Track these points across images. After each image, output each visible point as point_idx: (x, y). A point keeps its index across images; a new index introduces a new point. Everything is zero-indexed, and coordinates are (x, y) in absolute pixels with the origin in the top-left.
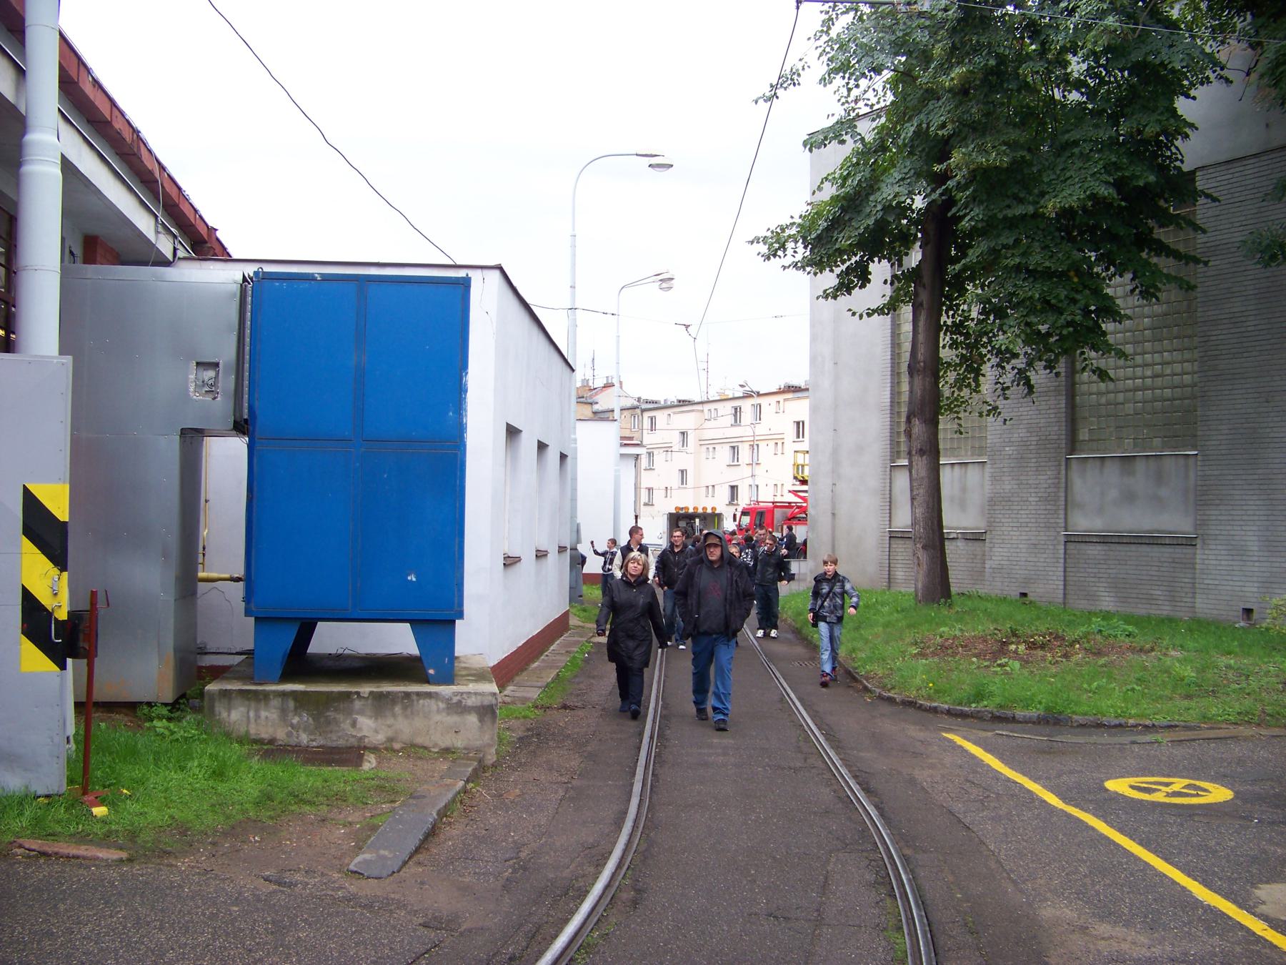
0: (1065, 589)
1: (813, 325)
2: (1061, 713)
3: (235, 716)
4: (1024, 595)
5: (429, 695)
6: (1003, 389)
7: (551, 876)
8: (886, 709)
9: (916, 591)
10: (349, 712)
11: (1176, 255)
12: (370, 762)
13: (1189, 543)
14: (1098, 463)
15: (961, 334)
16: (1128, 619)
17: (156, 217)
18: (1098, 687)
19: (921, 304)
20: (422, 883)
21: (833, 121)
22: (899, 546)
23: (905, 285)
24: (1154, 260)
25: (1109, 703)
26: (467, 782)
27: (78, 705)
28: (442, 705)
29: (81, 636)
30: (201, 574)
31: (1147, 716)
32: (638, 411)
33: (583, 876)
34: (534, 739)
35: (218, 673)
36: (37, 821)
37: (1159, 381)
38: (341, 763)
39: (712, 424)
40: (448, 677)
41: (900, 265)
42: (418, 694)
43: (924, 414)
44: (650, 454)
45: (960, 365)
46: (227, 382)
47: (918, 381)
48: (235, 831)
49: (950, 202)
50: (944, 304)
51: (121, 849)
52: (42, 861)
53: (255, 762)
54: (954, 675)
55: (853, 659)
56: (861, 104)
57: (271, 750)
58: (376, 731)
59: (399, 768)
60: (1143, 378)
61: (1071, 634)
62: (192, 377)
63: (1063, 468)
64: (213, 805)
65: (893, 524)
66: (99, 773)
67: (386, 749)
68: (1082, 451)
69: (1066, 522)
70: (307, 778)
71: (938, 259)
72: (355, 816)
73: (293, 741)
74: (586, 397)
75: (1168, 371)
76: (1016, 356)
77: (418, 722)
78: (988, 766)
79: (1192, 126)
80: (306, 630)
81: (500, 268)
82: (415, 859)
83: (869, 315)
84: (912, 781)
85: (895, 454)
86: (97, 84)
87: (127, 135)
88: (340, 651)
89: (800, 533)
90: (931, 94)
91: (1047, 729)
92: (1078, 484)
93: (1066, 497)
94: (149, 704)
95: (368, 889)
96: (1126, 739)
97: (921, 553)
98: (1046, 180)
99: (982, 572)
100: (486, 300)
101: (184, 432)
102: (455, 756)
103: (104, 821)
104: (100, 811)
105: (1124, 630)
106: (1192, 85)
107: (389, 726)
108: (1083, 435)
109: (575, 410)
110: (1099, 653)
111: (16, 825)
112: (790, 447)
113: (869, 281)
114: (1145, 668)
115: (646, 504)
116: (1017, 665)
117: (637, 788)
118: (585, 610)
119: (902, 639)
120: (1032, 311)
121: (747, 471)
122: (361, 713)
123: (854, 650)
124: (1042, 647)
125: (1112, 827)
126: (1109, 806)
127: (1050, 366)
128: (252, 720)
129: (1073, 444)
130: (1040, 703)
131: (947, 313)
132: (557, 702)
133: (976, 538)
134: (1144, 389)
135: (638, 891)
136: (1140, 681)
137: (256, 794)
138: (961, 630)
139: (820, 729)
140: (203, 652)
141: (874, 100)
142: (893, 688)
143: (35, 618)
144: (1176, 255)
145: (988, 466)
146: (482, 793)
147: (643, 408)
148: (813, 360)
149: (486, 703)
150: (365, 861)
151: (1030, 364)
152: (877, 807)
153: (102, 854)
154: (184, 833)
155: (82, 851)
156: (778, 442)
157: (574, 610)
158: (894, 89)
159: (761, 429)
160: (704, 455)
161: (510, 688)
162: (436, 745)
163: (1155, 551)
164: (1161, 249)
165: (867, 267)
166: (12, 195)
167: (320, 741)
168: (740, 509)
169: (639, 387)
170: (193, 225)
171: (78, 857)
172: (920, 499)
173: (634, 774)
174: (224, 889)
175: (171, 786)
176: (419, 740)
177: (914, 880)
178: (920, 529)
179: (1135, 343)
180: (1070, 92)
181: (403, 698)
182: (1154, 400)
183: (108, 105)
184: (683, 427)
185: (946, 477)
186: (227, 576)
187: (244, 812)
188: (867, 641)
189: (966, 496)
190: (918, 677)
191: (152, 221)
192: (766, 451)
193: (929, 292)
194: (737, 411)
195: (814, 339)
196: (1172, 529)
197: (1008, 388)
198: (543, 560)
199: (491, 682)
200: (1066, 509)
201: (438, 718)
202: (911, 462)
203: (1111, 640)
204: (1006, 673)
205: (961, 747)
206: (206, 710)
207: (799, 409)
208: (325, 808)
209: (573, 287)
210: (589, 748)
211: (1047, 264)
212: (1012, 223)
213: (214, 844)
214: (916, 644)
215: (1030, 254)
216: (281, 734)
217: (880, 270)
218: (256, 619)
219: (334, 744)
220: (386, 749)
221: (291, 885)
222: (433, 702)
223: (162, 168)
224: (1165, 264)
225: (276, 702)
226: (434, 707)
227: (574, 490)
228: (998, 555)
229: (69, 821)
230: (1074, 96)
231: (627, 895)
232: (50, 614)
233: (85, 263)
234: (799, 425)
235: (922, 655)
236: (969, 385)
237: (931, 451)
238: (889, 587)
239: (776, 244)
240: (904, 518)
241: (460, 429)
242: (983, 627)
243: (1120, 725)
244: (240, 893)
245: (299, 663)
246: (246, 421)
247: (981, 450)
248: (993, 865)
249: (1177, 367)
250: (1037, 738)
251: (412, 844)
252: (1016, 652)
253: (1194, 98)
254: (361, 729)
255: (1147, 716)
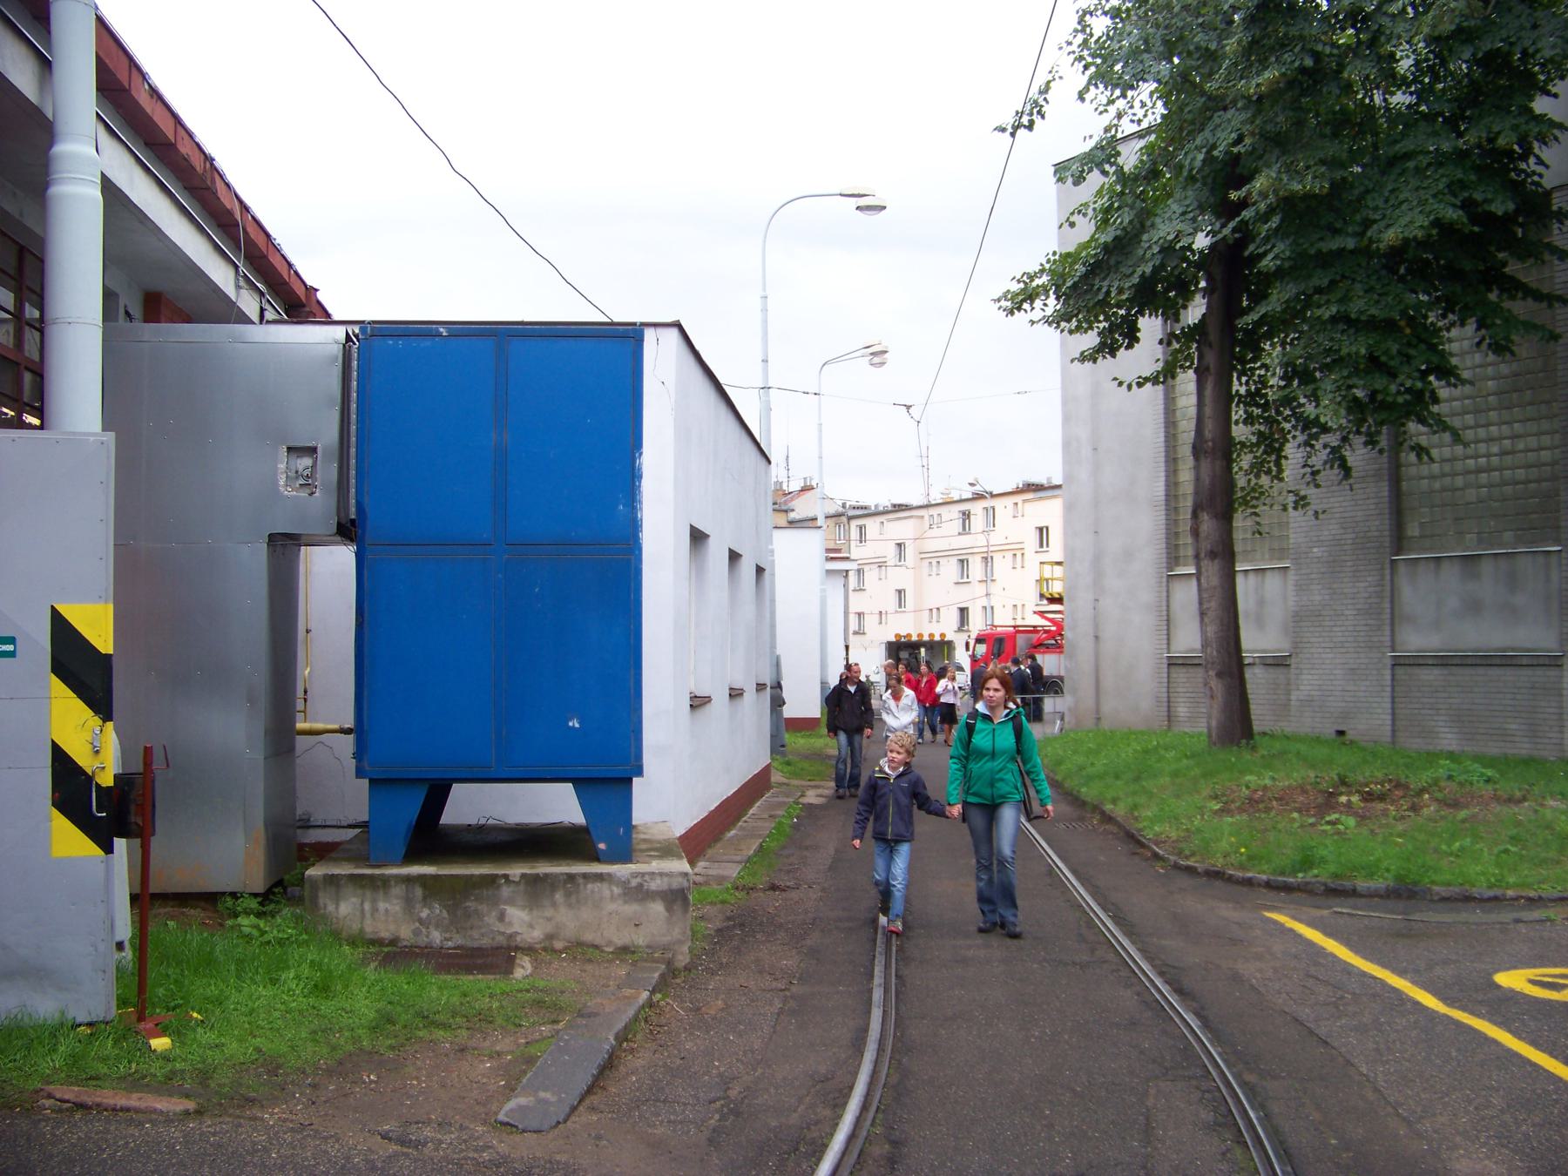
0: (1393, 724)
1: (1065, 403)
2: (1415, 883)
3: (346, 909)
4: (1341, 733)
5: (600, 877)
6: (1314, 473)
7: (774, 1124)
8: (1184, 881)
9: (1209, 728)
10: (495, 902)
11: (1538, 296)
12: (524, 968)
13: (1554, 663)
14: (1432, 565)
15: (1258, 406)
16: (1477, 758)
17: (236, 267)
18: (1462, 849)
19: (1207, 369)
20: (599, 1138)
21: (1091, 144)
22: (1180, 675)
23: (1179, 347)
24: (1506, 304)
25: (1479, 868)
26: (653, 992)
27: (134, 899)
28: (616, 890)
29: (133, 808)
30: (300, 725)
31: (1529, 886)
32: (844, 519)
33: (816, 1124)
34: (738, 929)
35: (324, 851)
36: (74, 1060)
37: (1508, 460)
38: (485, 969)
39: (935, 532)
40: (624, 853)
41: (1177, 320)
42: (585, 876)
43: (1213, 509)
44: (859, 572)
45: (1258, 445)
46: (328, 472)
47: (1206, 465)
48: (344, 1067)
49: (1245, 234)
50: (1234, 368)
51: (187, 1096)
52: (78, 1116)
53: (370, 972)
54: (1271, 836)
55: (1136, 819)
56: (1125, 120)
57: (394, 954)
58: (531, 926)
59: (563, 976)
60: (1488, 456)
61: (1416, 782)
62: (282, 466)
63: (1387, 572)
64: (315, 1032)
65: (1173, 648)
66: (161, 991)
67: (545, 949)
68: (1410, 551)
69: (1393, 641)
70: (440, 991)
71: (1226, 310)
72: (504, 1044)
73: (422, 941)
74: (781, 503)
75: (1521, 446)
76: (1325, 429)
77: (586, 914)
78: (1334, 956)
79: (1561, 126)
80: (438, 794)
81: (678, 325)
82: (587, 1102)
83: (1140, 385)
84: (1236, 978)
85: (1173, 559)
86: (155, 93)
87: (198, 164)
88: (483, 821)
89: (1049, 664)
90: (1217, 103)
91: (1401, 904)
92: (1406, 592)
93: (1392, 609)
94: (234, 895)
95: (523, 1148)
96: (1507, 916)
97: (1216, 684)
98: (1371, 204)
99: (1286, 705)
100: (661, 363)
101: (272, 538)
102: (636, 957)
103: (166, 1057)
104: (160, 1043)
105: (1482, 775)
106: (1549, 80)
107: (549, 919)
108: (1413, 530)
109: (772, 518)
110: (1455, 805)
111: (46, 1065)
112: (1033, 560)
113: (1137, 340)
114: (1518, 824)
115: (855, 633)
116: (1351, 822)
117: (878, 995)
118: (788, 763)
119: (1198, 792)
120: (1357, 372)
121: (980, 590)
122: (511, 902)
123: (1135, 807)
124: (1382, 798)
125: (1520, 1038)
126: (1506, 1007)
127: (1371, 441)
128: (368, 915)
129: (1399, 541)
130: (1388, 870)
131: (1239, 379)
132: (761, 881)
133: (1279, 663)
134: (1488, 469)
135: (895, 1144)
136: (1514, 839)
137: (372, 1015)
138: (1273, 778)
139: (1104, 909)
140: (306, 825)
141: (1140, 113)
142: (1193, 854)
143: (70, 786)
144: (1538, 296)
145: (1291, 573)
146: (675, 1008)
147: (849, 516)
148: (1067, 445)
149: (675, 886)
150: (521, 1108)
151: (1345, 439)
152: (1197, 1015)
153: (162, 1104)
154: (273, 1072)
155: (134, 1101)
156: (1017, 553)
157: (775, 764)
158: (1165, 97)
159: (996, 538)
160: (925, 570)
161: (701, 864)
162: (610, 943)
163: (1509, 675)
164: (1513, 287)
165: (1135, 322)
166: (37, 230)
167: (458, 940)
168: (974, 635)
169: (844, 490)
170: (286, 283)
171: (128, 1110)
172: (1211, 614)
173: (872, 976)
174: (326, 1152)
175: (259, 1008)
176: (588, 937)
177: (1267, 1118)
178: (1213, 652)
179: (1477, 411)
180: (1392, 94)
181: (565, 882)
182: (1504, 483)
183: (171, 122)
184: (899, 537)
185: (1245, 588)
186: (336, 726)
187: (356, 1040)
188: (1151, 795)
189: (1268, 608)
190: (1226, 840)
191: (231, 273)
192: (1001, 564)
193: (1219, 351)
194: (966, 515)
195: (1067, 419)
196: (1529, 646)
197: (1318, 472)
198: (738, 701)
199: (680, 857)
200: (1392, 624)
201: (611, 907)
202: (1199, 568)
203: (1468, 788)
204: (1338, 833)
205: (1291, 930)
206: (307, 902)
207: (1049, 511)
208: (464, 1033)
209: (765, 361)
210: (809, 942)
211: (1373, 311)
212: (1325, 260)
213: (314, 1086)
214: (1216, 797)
215: (1350, 300)
216: (406, 932)
217: (1150, 327)
218: (372, 781)
219: (476, 944)
220: (545, 949)
221: (418, 1144)
222: (605, 886)
223: (245, 208)
224: (1520, 308)
225: (398, 890)
226: (607, 893)
227: (773, 613)
228: (1307, 683)
229: (118, 1058)
230: (1400, 99)
231: (880, 1150)
232: (89, 779)
233: (146, 321)
234: (1042, 531)
235: (1225, 811)
236: (1268, 472)
237: (1225, 553)
238: (1169, 727)
239: (1022, 298)
240: (1189, 638)
241: (634, 526)
242: (1299, 774)
243: (1496, 898)
244: (348, 1158)
245: (430, 838)
246: (353, 522)
247: (1281, 553)
248: (1370, 1095)
249: (1532, 442)
250: (1386, 916)
251: (583, 1080)
252: (1349, 804)
253: (1555, 96)
254: (510, 924)
255: (1529, 886)
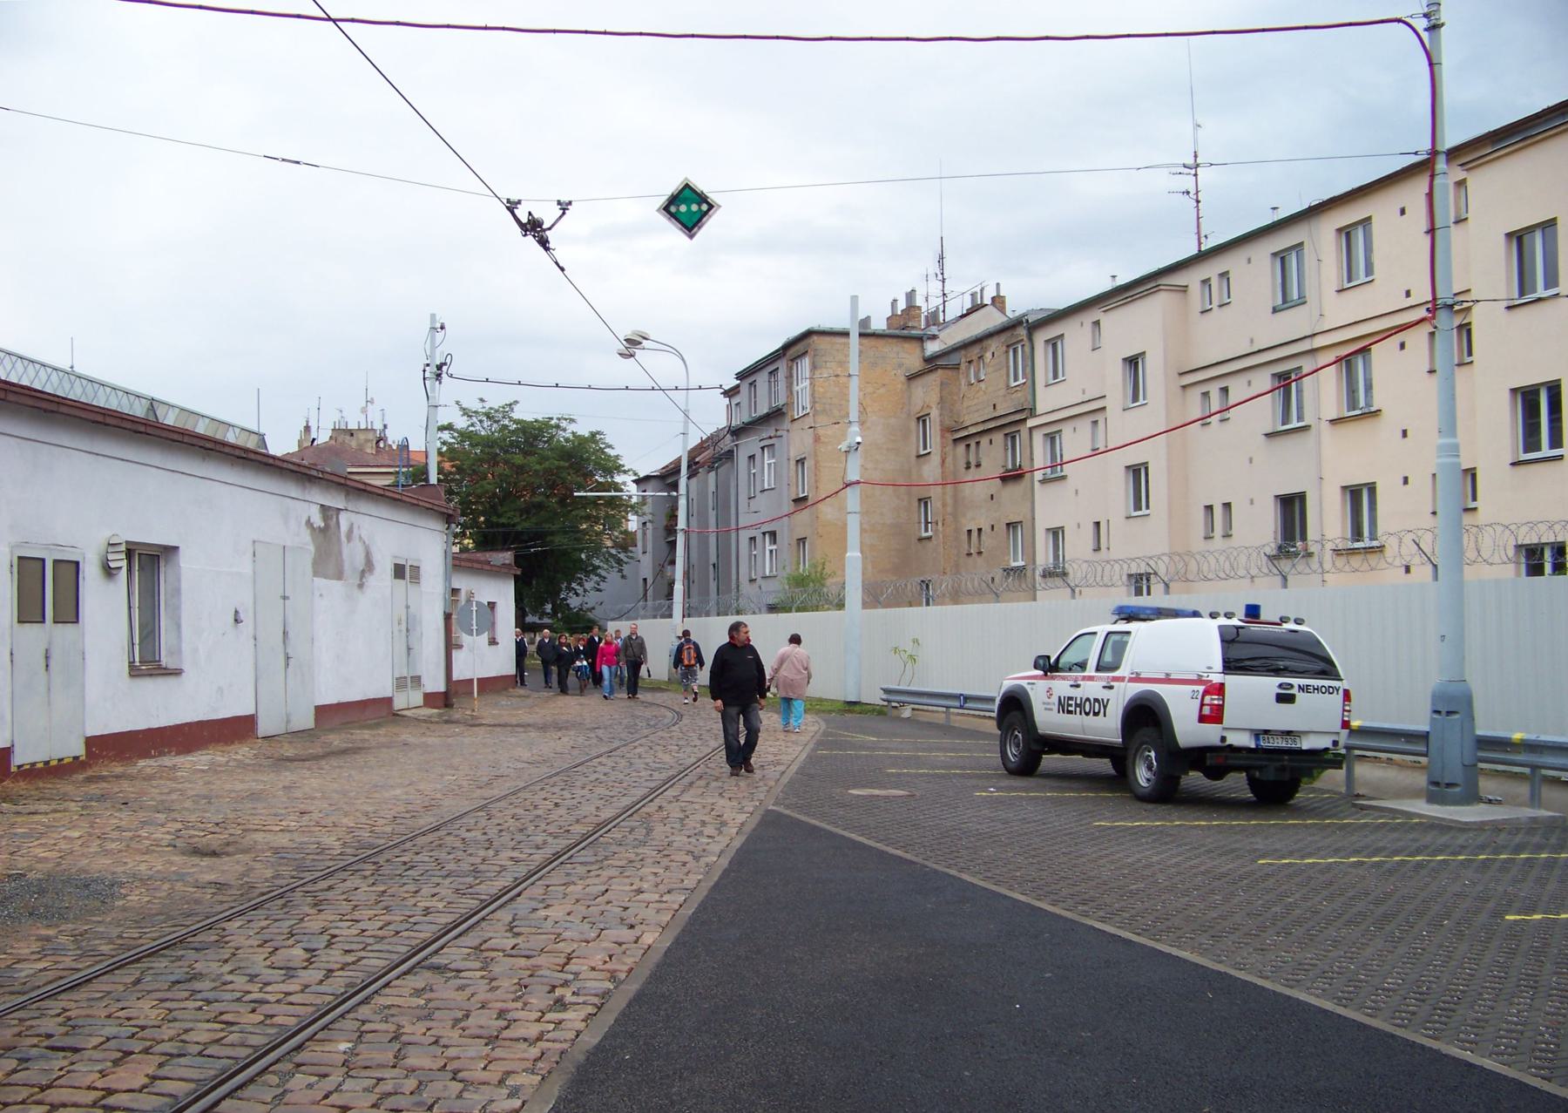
32: (1022, 332)
